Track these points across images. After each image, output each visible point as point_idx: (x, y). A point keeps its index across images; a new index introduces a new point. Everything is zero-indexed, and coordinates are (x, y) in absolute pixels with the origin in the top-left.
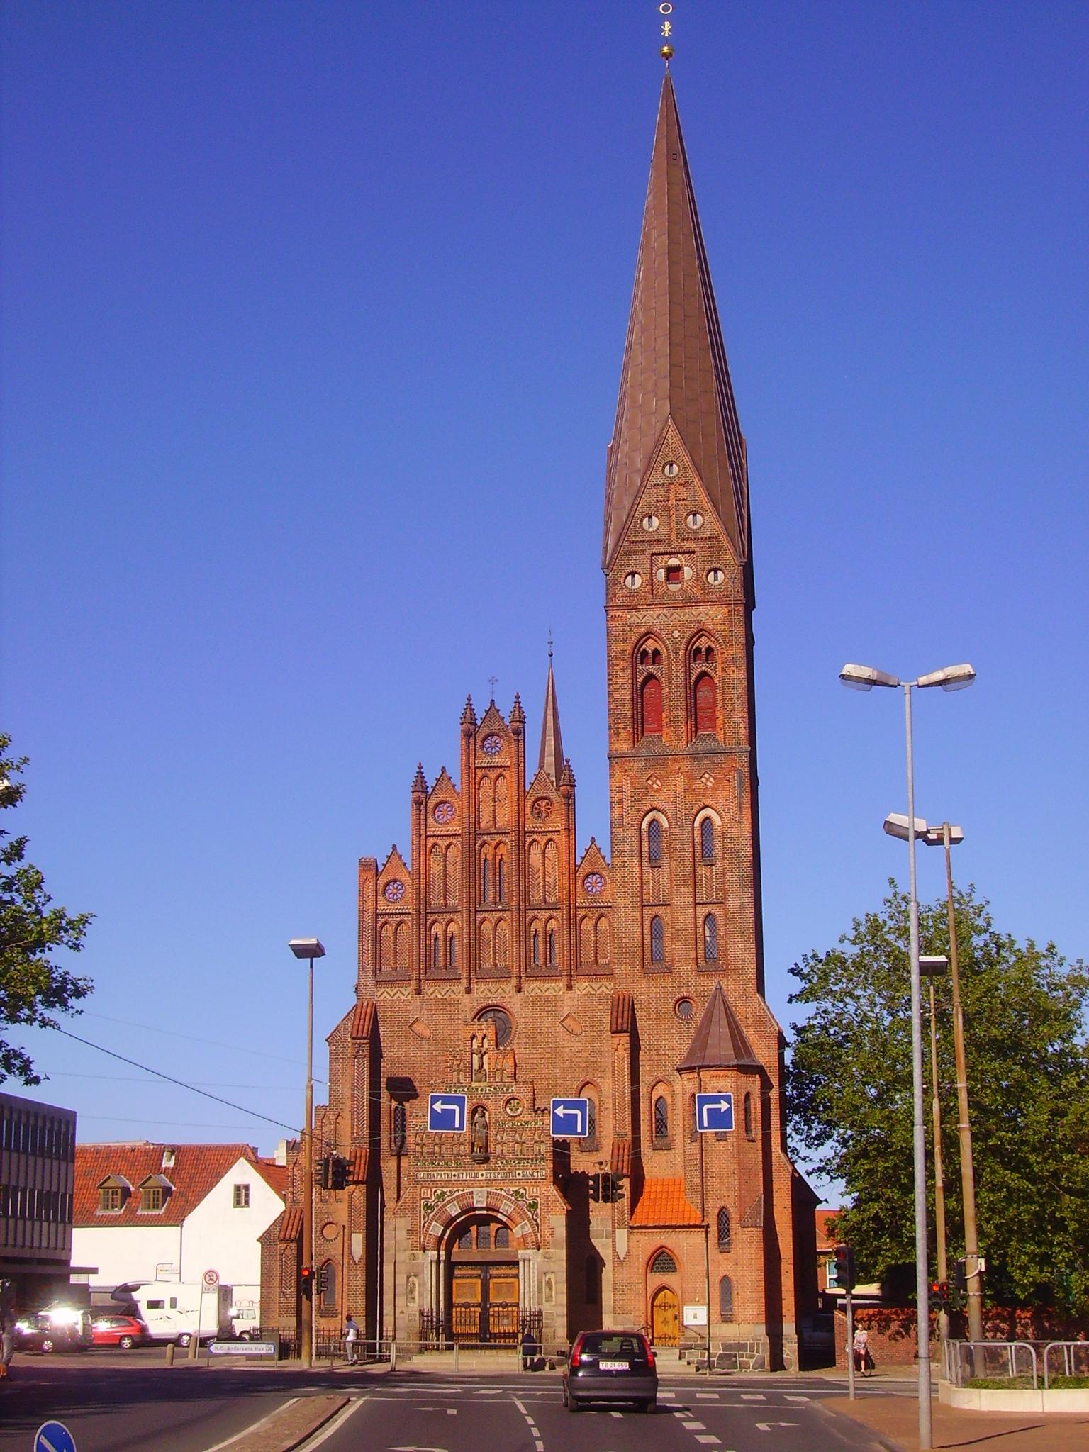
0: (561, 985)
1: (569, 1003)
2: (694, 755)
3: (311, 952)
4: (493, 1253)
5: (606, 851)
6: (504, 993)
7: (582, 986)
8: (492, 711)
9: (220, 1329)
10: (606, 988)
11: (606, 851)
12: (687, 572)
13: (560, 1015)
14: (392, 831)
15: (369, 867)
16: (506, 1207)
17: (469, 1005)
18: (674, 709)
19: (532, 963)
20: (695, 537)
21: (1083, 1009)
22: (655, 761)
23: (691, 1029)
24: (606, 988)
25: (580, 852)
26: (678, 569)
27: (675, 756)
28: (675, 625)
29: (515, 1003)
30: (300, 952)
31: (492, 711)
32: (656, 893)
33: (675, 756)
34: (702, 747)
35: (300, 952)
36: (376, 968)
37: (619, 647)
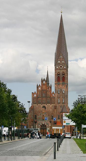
0: (46, 104)
1: (51, 106)
2: (63, 84)
3: (29, 102)
4: (44, 128)
5: (54, 92)
6: (45, 105)
7: (52, 105)
8: (44, 79)
9: (76, 108)
10: (54, 105)
11: (54, 92)
12: (62, 67)
13: (50, 107)
14: (35, 90)
15: (33, 93)
16: (46, 124)
17: (42, 106)
18: (61, 79)
19: (47, 103)
20: (63, 63)
21: (18, 100)
22: (59, 84)
23: (62, 108)
24: (54, 105)
25: (52, 92)
26: (61, 66)
27: (61, 84)
28: (61, 72)
29: (46, 106)
30: (28, 102)
31: (44, 79)
32: (59, 96)
33: (61, 84)
34: (63, 83)
35: (28, 102)
36: (33, 103)
37: (56, 73)
